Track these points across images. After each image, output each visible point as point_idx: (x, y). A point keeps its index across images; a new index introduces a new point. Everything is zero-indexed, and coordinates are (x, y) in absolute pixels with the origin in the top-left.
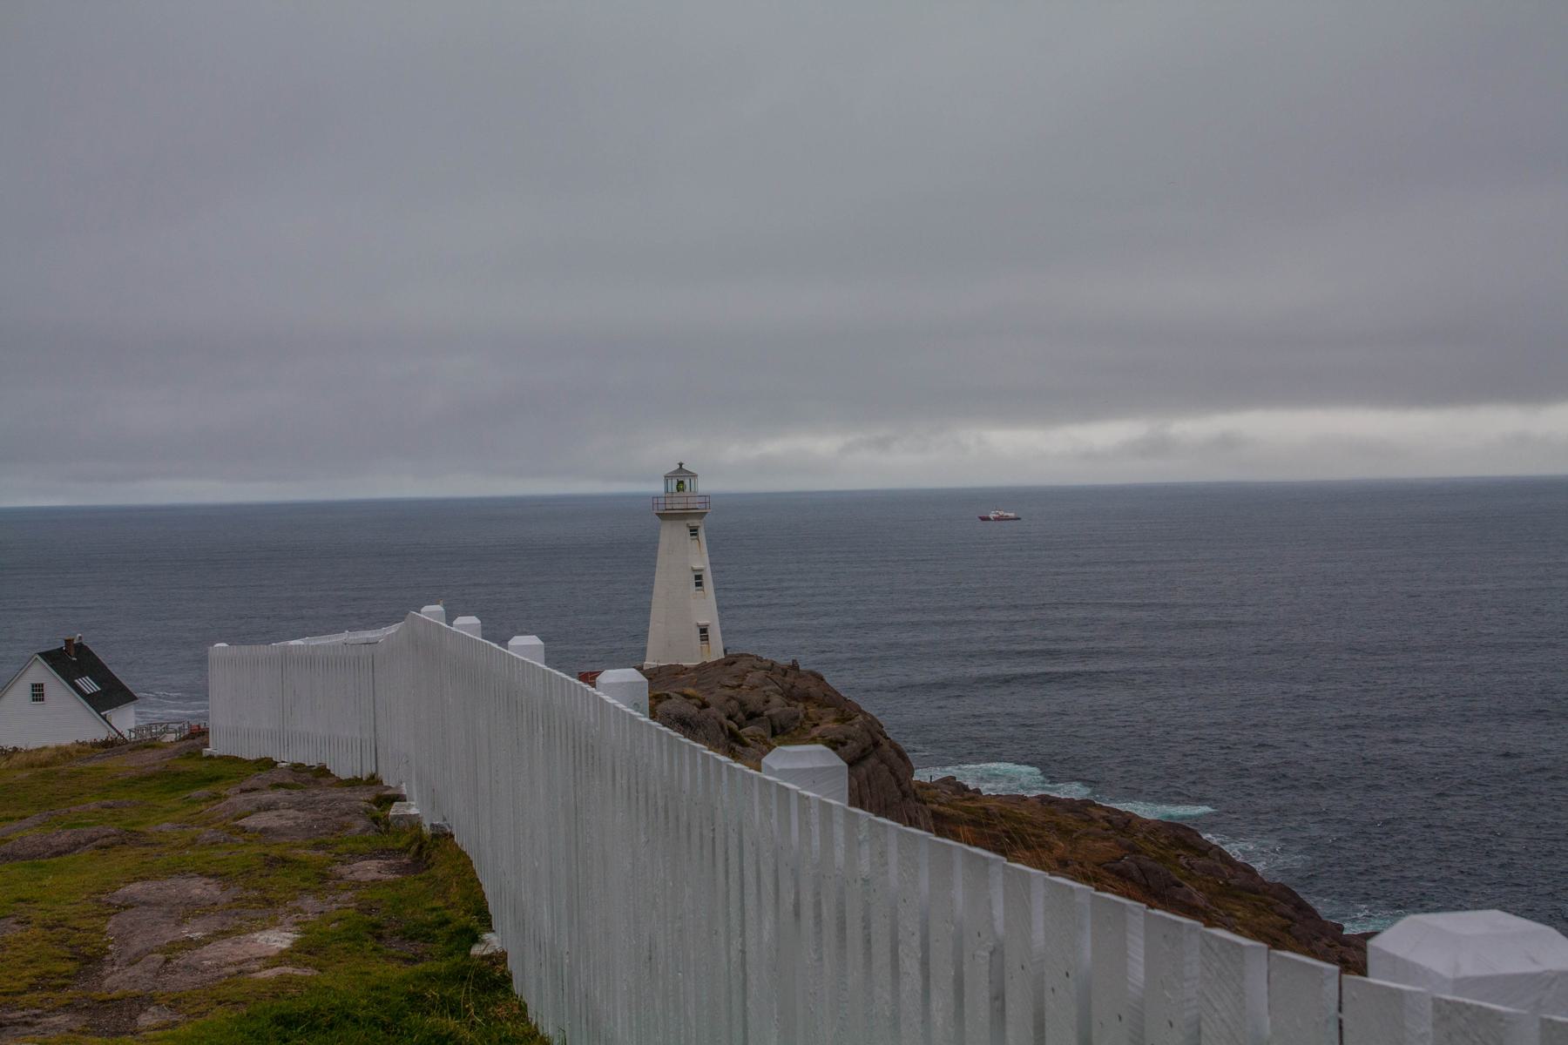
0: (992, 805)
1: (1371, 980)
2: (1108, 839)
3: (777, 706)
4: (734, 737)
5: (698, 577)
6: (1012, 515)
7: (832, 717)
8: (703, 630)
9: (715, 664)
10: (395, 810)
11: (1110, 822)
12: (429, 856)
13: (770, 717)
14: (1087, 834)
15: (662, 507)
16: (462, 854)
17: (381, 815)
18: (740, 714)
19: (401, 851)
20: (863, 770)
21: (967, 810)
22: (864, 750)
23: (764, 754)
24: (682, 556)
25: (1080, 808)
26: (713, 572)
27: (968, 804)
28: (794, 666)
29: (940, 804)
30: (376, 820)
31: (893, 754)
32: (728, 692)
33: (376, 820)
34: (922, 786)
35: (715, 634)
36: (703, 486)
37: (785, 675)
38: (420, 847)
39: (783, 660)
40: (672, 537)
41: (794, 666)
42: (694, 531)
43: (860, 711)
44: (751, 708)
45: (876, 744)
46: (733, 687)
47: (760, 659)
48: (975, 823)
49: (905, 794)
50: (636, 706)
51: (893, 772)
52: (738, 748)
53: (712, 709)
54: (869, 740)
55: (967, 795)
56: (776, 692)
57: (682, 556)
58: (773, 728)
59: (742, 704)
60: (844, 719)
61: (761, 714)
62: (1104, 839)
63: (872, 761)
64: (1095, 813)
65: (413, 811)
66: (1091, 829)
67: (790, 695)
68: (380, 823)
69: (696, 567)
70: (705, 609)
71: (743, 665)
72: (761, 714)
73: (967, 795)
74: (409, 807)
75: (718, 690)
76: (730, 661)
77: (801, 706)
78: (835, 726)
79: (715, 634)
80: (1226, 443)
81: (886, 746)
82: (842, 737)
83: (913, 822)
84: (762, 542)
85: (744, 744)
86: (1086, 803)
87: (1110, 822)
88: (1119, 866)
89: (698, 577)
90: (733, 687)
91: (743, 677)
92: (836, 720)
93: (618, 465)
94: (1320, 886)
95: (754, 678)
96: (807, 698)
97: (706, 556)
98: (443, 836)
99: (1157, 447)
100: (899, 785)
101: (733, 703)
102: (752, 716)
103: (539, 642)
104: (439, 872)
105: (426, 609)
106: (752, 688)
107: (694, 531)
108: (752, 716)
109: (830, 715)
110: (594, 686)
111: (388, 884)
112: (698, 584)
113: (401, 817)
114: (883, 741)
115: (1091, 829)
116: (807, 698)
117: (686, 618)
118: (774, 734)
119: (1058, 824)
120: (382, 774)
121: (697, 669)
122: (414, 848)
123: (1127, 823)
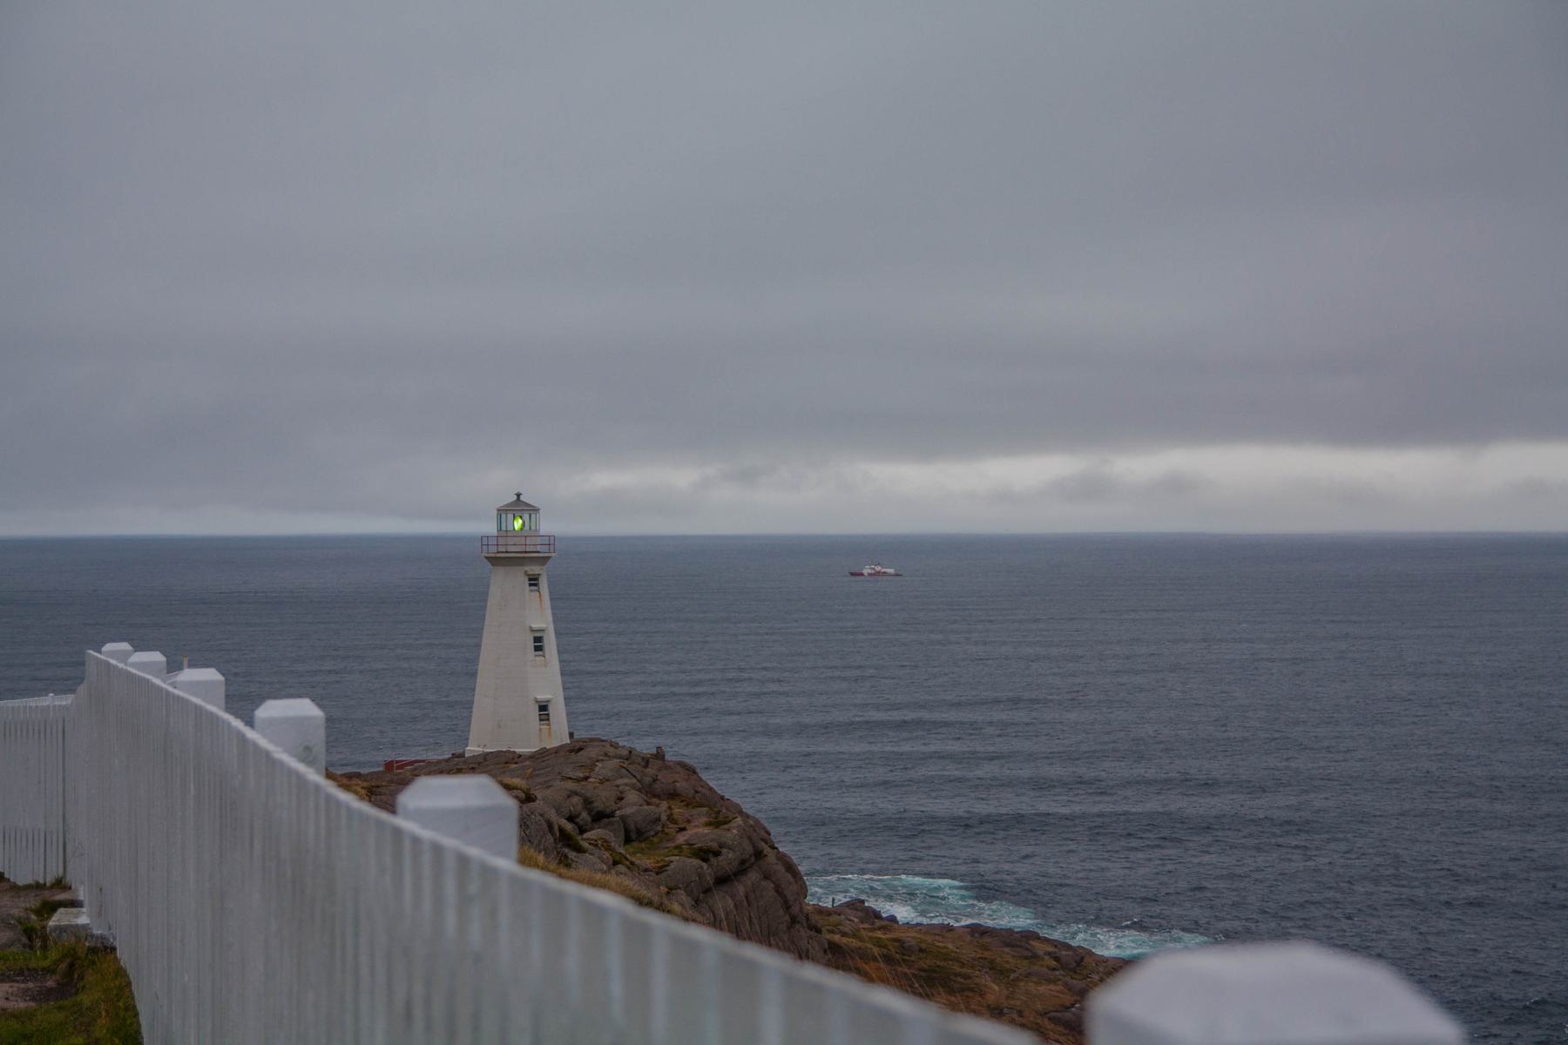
0: (910, 937)
1: (398, 821)
2: (1055, 981)
3: (633, 805)
4: (565, 839)
5: (538, 640)
6: (891, 571)
7: (704, 819)
8: (543, 708)
9: (557, 750)
10: (59, 918)
11: (1057, 959)
12: (81, 978)
13: (623, 818)
14: (1028, 975)
15: (494, 549)
16: (120, 973)
17: (37, 926)
18: (584, 815)
19: (48, 971)
21: (879, 943)
22: (743, 862)
23: (398, 791)
24: (518, 612)
25: (1020, 941)
26: (558, 634)
27: (879, 934)
28: (659, 755)
29: (844, 934)
30: (29, 932)
31: (780, 868)
32: (570, 785)
33: (29, 932)
34: (821, 911)
35: (558, 711)
36: (548, 526)
37: (646, 766)
38: (71, 966)
39: (645, 746)
40: (505, 586)
41: (659, 755)
42: (534, 581)
43: (741, 813)
44: (598, 805)
45: (759, 855)
46: (578, 780)
47: (615, 746)
48: (888, 959)
49: (794, 920)
50: (307, 756)
51: (778, 890)
52: (572, 855)
53: (538, 805)
54: (750, 849)
55: (878, 923)
56: (633, 787)
57: (518, 612)
58: (627, 831)
59: (587, 802)
60: (718, 822)
61: (612, 815)
62: (1049, 981)
63: (753, 876)
64: (1040, 948)
65: (83, 920)
66: (1034, 968)
67: (650, 792)
68: (32, 935)
69: (535, 626)
70: (546, 681)
71: (593, 752)
72: (612, 815)
73: (878, 923)
74: (77, 916)
75: (558, 784)
77: (664, 805)
78: (706, 830)
79: (558, 711)
80: (1176, 485)
81: (771, 857)
82: (714, 845)
83: (803, 955)
84: (618, 596)
85: (579, 850)
86: (1029, 935)
87: (1057, 959)
88: (1068, 1015)
89: (538, 640)
90: (578, 780)
91: (592, 767)
92: (708, 824)
93: (443, 496)
95: (604, 769)
96: (673, 795)
97: (549, 612)
98: (105, 949)
99: (1090, 489)
100: (787, 906)
101: (575, 799)
102: (599, 817)
103: (221, 678)
104: (85, 999)
105: (108, 647)
106: (601, 782)
107: (534, 581)
108: (599, 817)
109: (701, 816)
110: (250, 723)
111: (15, 1016)
112: (538, 649)
113: (61, 929)
114: (767, 850)
115: (1034, 968)
116: (673, 795)
117: (520, 690)
118: (628, 840)
119: (992, 961)
120: (70, 878)
121: (532, 757)
122: (63, 966)
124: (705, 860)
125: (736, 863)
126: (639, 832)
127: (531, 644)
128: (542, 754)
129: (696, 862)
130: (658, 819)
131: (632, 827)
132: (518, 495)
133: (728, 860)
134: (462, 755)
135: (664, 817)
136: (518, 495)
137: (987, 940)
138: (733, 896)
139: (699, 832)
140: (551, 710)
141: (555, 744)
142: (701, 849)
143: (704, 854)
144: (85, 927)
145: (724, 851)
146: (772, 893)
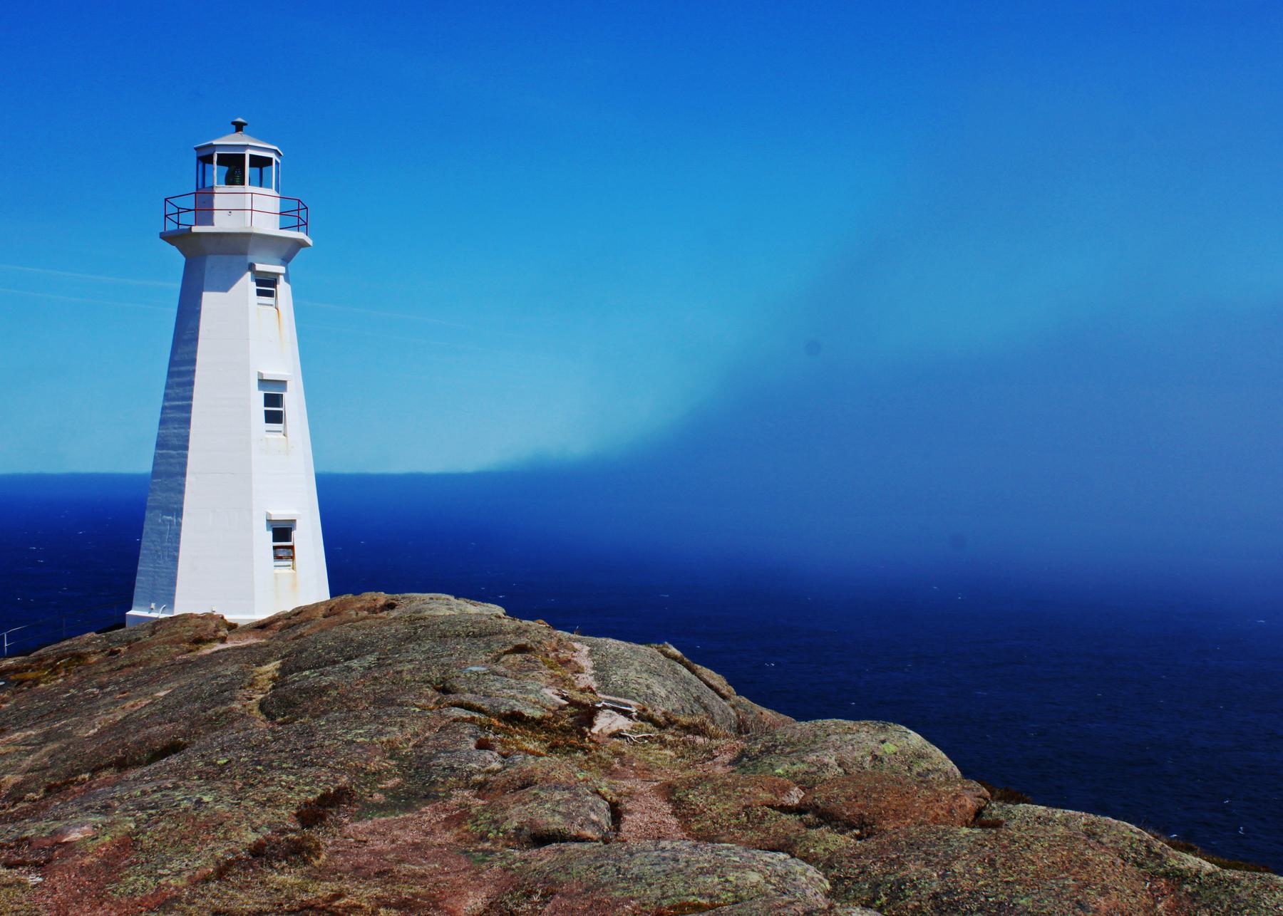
5: (273, 400)
42: (266, 285)
89: (273, 400)
123: (66, 718)
127: (259, 408)
140: (297, 537)
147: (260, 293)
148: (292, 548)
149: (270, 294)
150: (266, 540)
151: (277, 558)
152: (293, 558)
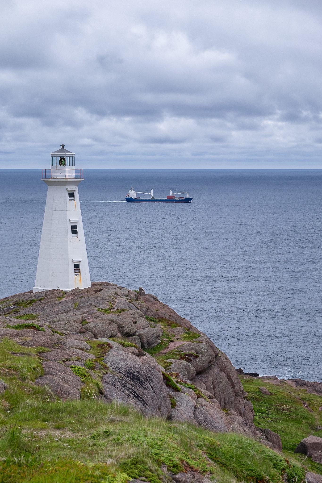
5: (74, 227)
8: (77, 266)
9: (88, 290)
13: (140, 336)
20: (210, 378)
22: (210, 362)
39: (134, 288)
41: (141, 293)
42: (71, 195)
44: (127, 329)
45: (216, 356)
49: (237, 394)
58: (142, 344)
63: (216, 370)
69: (72, 220)
70: (78, 249)
71: (108, 293)
72: (134, 334)
76: (98, 288)
79: (85, 267)
82: (194, 352)
89: (74, 227)
92: (185, 338)
94: (27, 242)
100: (233, 386)
107: (71, 195)
112: (74, 232)
124: (189, 360)
125: (207, 362)
126: (149, 344)
127: (70, 230)
128: (76, 293)
129: (184, 362)
130: (159, 336)
131: (145, 341)
132: (63, 146)
133: (202, 360)
134: (31, 292)
135: (161, 335)
136: (63, 146)
137: (305, 388)
138: (205, 383)
139: (180, 343)
140: (81, 267)
141: (312, 380)
142: (186, 355)
143: (188, 357)
144: (178, 478)
145: (200, 355)
146: (226, 379)
147: (70, 197)
148: (80, 269)
149: (72, 197)
150: (72, 268)
151: (75, 272)
152: (80, 272)
